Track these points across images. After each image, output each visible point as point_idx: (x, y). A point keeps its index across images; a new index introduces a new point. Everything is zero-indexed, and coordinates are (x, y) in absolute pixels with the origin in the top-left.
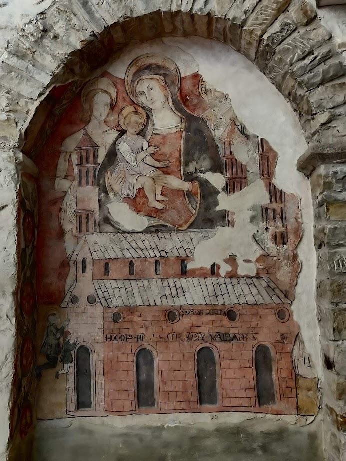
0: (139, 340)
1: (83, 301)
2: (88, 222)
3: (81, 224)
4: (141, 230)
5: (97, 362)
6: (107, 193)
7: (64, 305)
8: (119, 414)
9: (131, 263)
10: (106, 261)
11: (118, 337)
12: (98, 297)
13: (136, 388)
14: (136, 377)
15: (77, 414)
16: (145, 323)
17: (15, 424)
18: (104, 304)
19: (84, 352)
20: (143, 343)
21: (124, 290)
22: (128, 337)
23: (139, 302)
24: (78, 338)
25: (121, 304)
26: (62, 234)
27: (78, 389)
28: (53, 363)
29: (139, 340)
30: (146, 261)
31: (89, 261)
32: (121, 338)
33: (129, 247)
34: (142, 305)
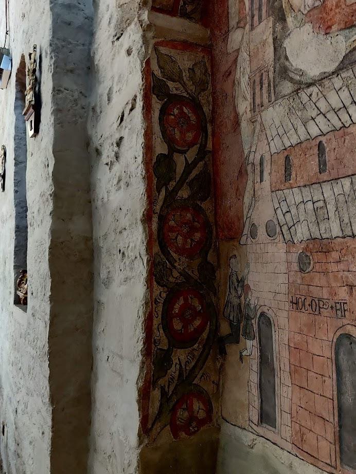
0: (339, 312)
1: (262, 232)
2: (261, 88)
3: (254, 89)
4: (331, 68)
5: (281, 339)
6: (282, 19)
7: (244, 238)
8: (311, 460)
9: (320, 146)
10: (286, 153)
11: (307, 303)
12: (279, 223)
13: (336, 419)
14: (335, 393)
15: (260, 430)
16: (347, 277)
17: (154, 409)
18: (288, 237)
19: (266, 321)
20: (345, 321)
21: (310, 205)
22: (321, 303)
23: (336, 231)
24: (258, 298)
25: (307, 235)
26: (237, 123)
27: (261, 387)
28: (234, 338)
29: (339, 312)
30: (345, 134)
31: (267, 157)
32: (311, 305)
33: (314, 113)
34: (341, 235)
